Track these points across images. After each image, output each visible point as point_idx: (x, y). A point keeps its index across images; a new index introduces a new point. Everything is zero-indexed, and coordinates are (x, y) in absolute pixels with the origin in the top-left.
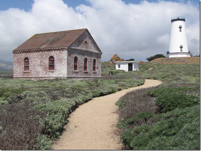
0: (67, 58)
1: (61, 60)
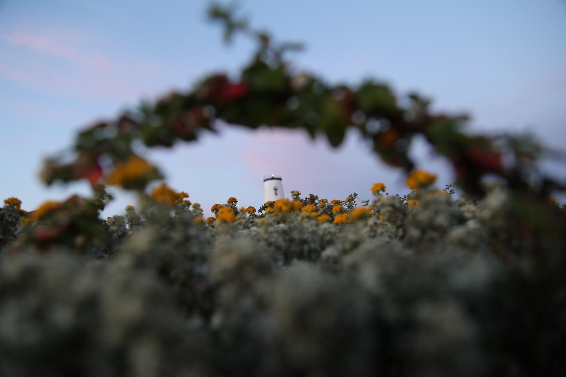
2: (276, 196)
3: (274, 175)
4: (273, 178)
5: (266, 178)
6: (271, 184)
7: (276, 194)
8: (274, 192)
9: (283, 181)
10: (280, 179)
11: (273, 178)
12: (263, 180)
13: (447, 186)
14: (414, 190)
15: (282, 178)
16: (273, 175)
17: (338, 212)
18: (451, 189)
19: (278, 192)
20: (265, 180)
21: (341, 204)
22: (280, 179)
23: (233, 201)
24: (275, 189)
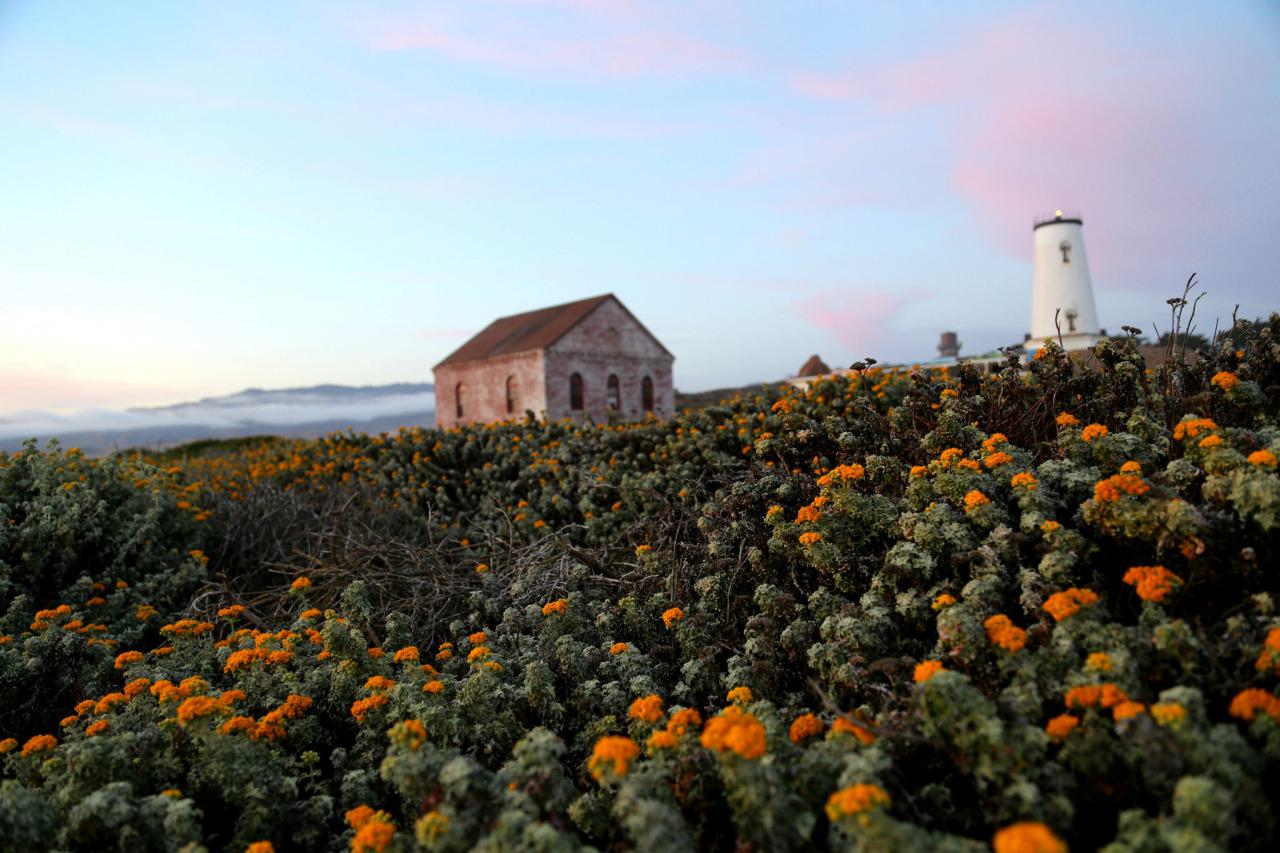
0: (547, 378)
1: (531, 385)
2: (1067, 265)
3: (1062, 211)
4: (1058, 221)
5: (1040, 221)
6: (1050, 236)
7: (1066, 260)
8: (1059, 256)
9: (1084, 228)
10: (1078, 222)
11: (1058, 221)
12: (1032, 225)
13: (1126, 329)
14: (1224, 796)
15: (1085, 222)
16: (1059, 213)
17: (750, 701)
18: (1039, 730)
19: (1071, 255)
20: (1037, 227)
21: (394, 713)
22: (1078, 222)
23: (950, 343)
24: (1064, 249)
